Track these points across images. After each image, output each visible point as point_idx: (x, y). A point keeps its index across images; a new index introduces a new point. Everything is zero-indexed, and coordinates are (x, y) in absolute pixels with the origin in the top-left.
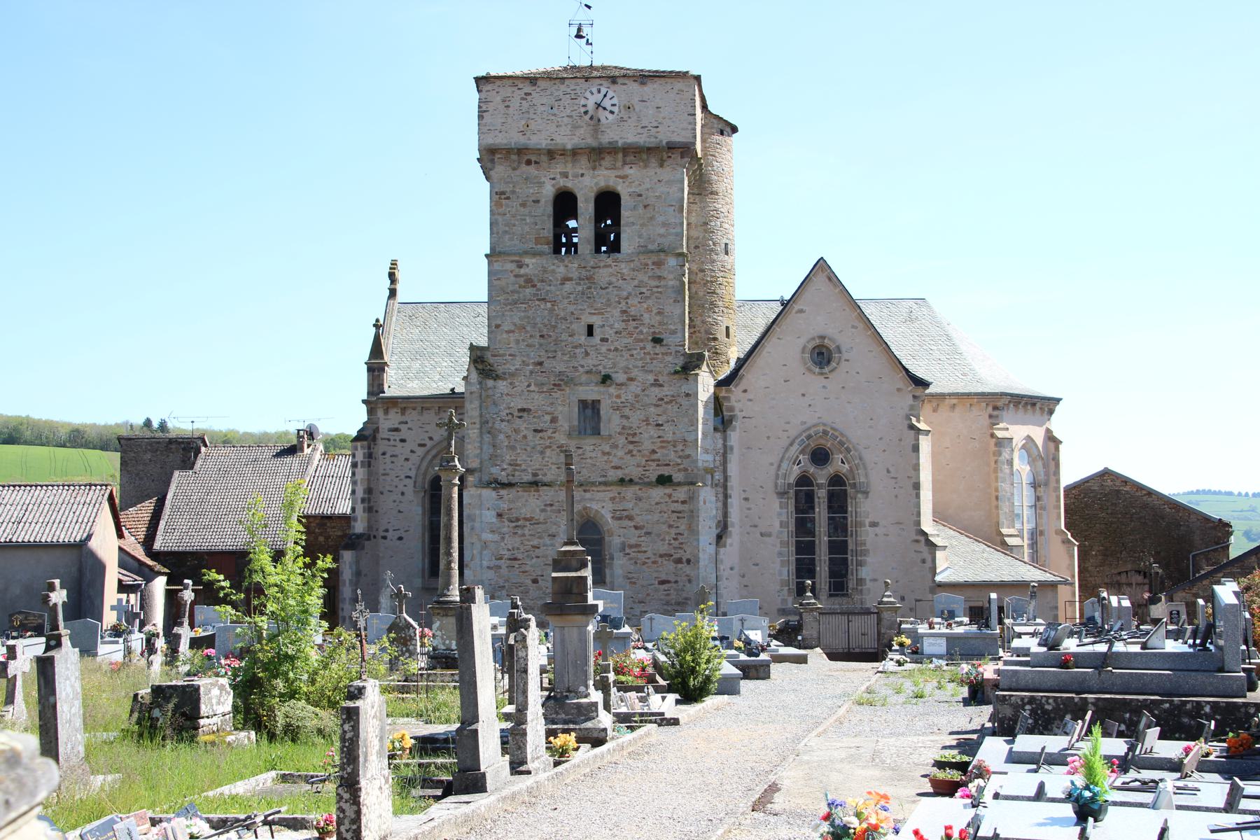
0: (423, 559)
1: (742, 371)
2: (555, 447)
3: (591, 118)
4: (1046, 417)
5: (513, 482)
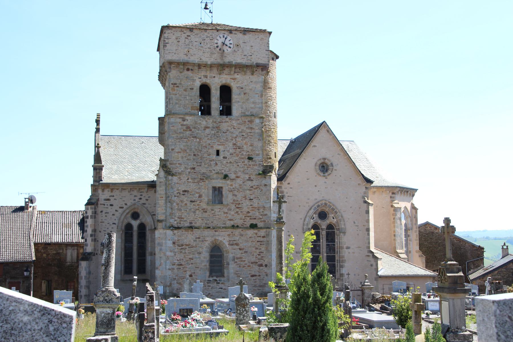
0: (121, 265)
1: (288, 174)
2: (200, 209)
3: (220, 50)
4: (411, 197)
5: (180, 226)
